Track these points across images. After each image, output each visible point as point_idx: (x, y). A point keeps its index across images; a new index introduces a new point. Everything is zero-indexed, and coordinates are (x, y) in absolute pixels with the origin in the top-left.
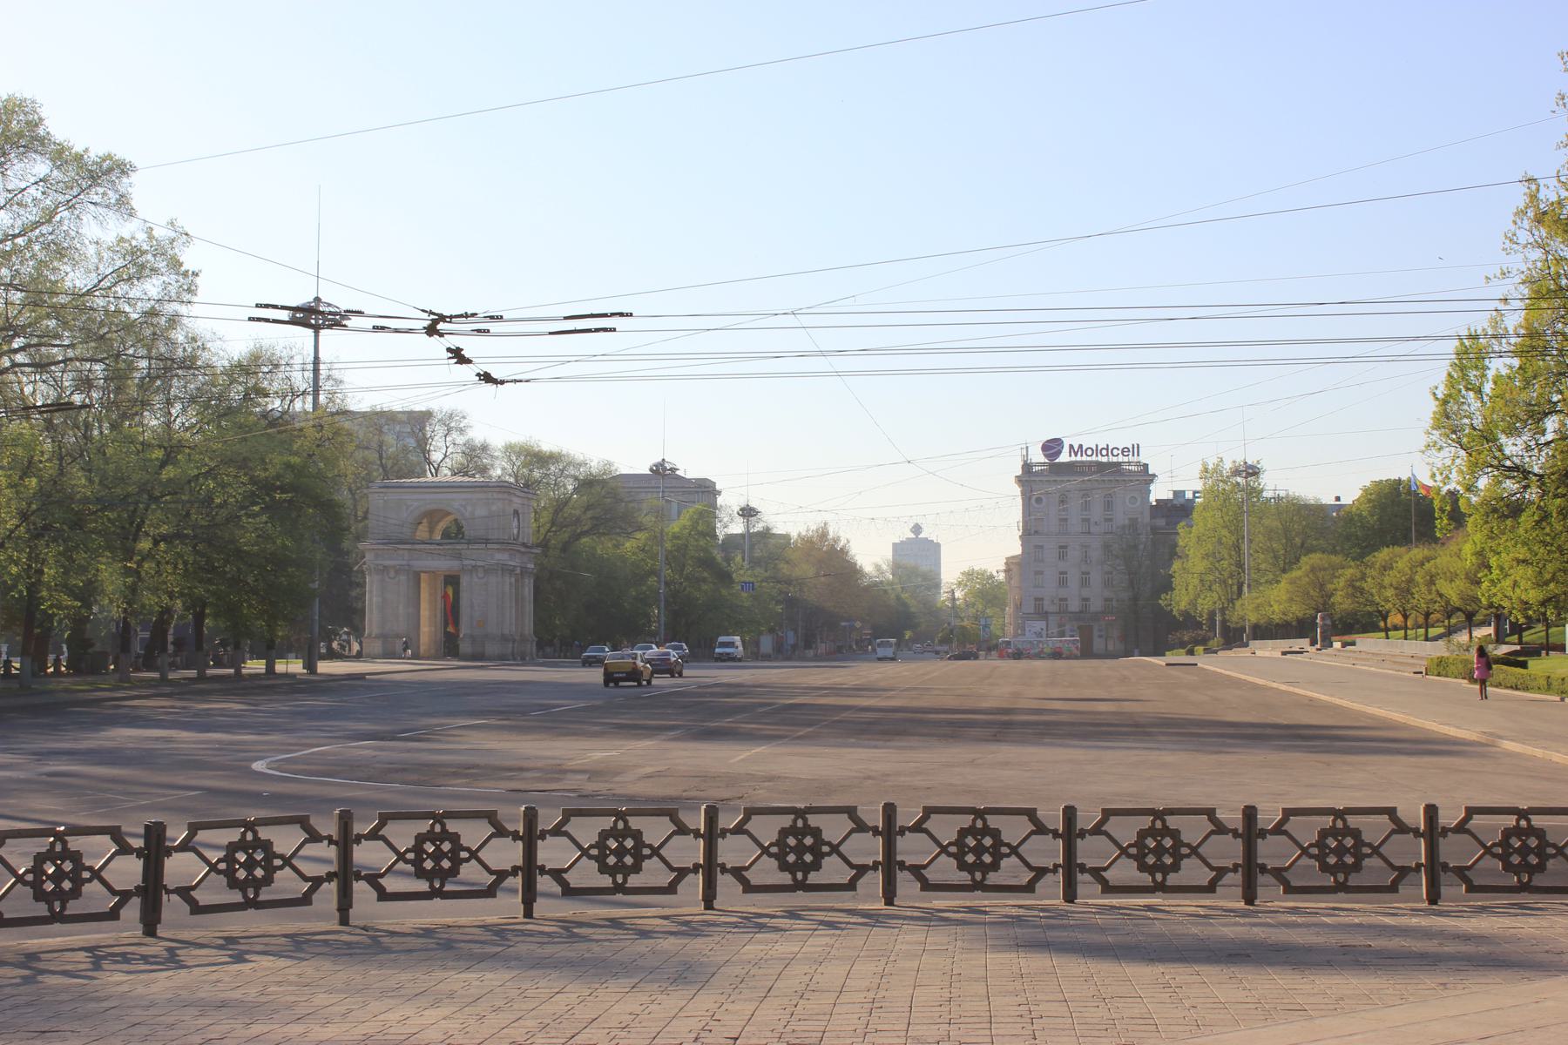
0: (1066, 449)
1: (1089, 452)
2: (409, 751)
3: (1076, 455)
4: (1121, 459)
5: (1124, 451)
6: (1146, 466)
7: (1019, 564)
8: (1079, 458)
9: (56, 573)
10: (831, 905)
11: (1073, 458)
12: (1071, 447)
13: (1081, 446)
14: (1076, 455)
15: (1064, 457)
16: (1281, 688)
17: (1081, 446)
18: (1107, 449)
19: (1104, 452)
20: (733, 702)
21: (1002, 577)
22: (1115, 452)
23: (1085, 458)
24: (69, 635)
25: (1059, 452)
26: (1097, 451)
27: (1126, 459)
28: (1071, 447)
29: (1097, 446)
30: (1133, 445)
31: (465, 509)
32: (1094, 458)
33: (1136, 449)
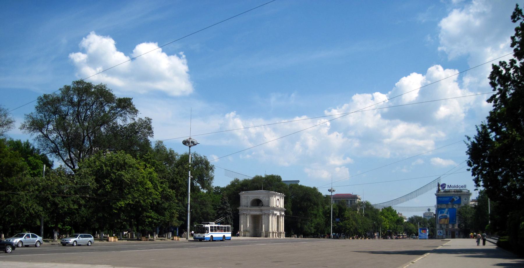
0: (447, 187)
1: (453, 187)
2: (282, 226)
3: (449, 187)
4: (461, 188)
5: (462, 187)
6: (469, 191)
7: (118, 49)
8: (450, 189)
9: (46, 191)
10: (128, 241)
11: (449, 189)
12: (448, 186)
13: (451, 186)
14: (449, 187)
15: (446, 188)
16: (442, 160)
17: (451, 186)
18: (457, 186)
19: (457, 187)
20: (133, 242)
21: (342, 134)
22: (460, 187)
23: (452, 189)
24: (518, 111)
25: (445, 187)
26: (455, 187)
27: (462, 189)
28: (448, 186)
29: (455, 185)
30: (464, 185)
31: (263, 198)
32: (454, 189)
33: (465, 186)
